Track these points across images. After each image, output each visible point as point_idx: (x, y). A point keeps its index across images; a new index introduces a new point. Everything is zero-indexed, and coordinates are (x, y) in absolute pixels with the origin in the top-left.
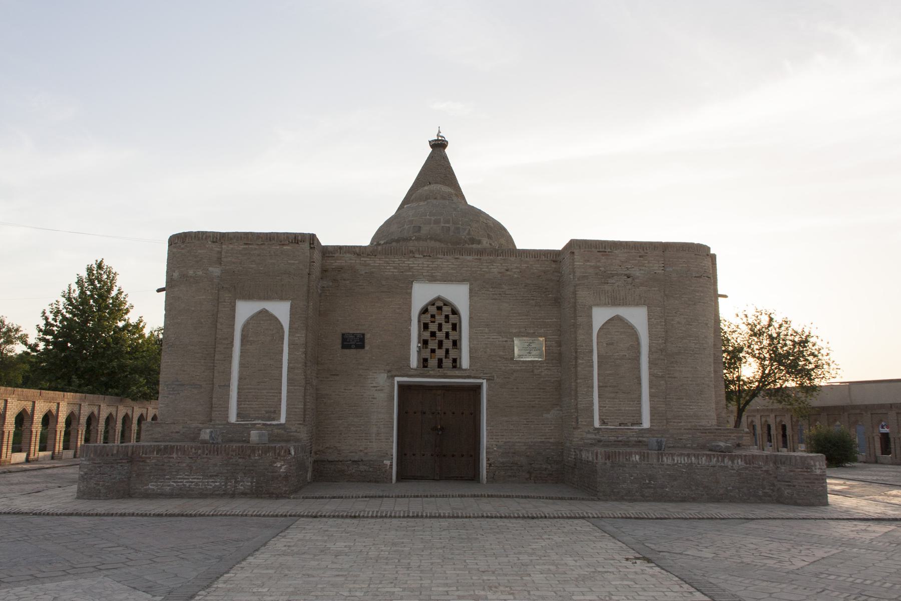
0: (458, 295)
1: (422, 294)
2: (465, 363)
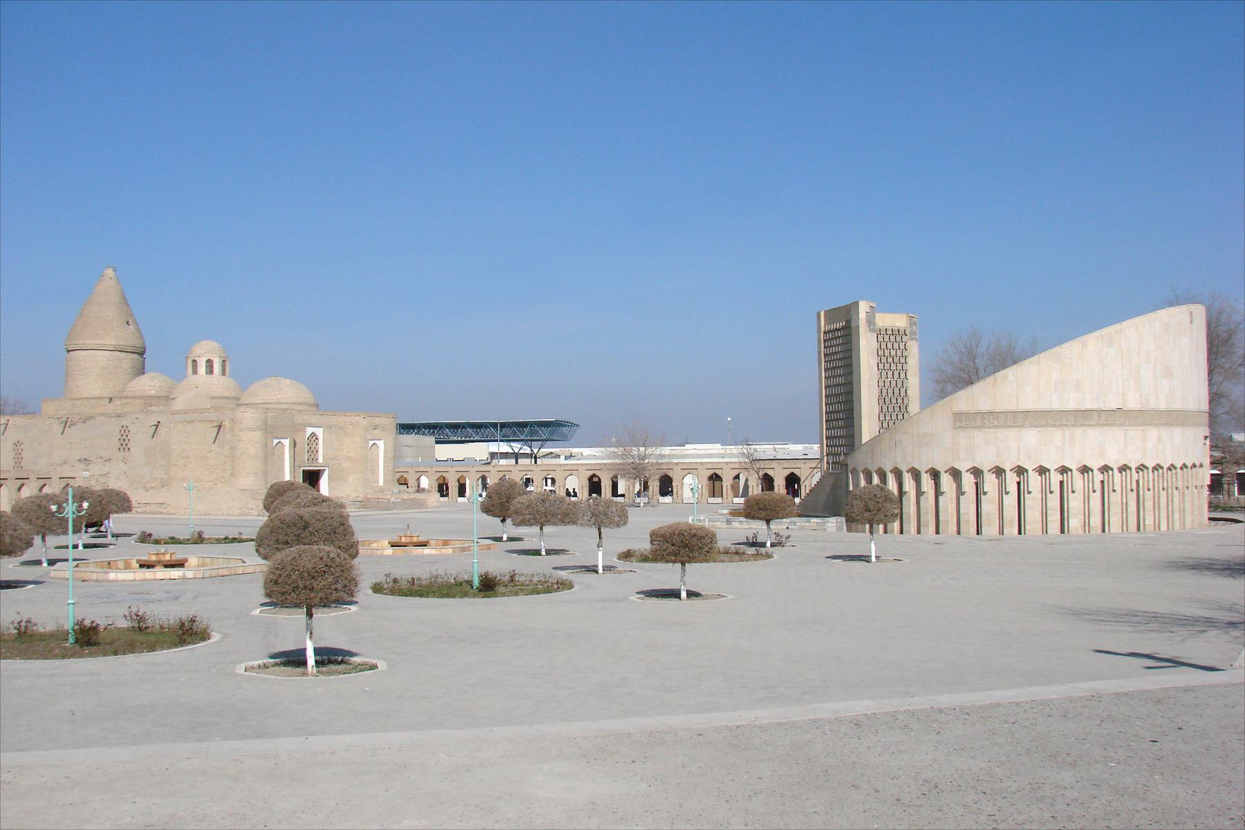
0: (319, 432)
1: (309, 431)
2: (321, 460)
